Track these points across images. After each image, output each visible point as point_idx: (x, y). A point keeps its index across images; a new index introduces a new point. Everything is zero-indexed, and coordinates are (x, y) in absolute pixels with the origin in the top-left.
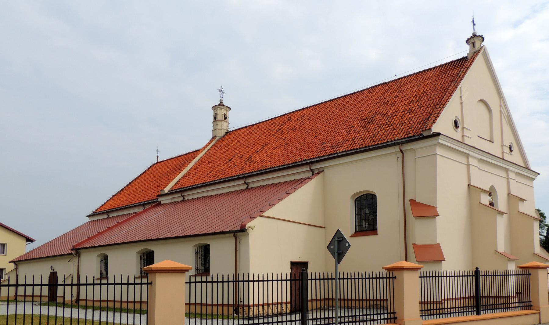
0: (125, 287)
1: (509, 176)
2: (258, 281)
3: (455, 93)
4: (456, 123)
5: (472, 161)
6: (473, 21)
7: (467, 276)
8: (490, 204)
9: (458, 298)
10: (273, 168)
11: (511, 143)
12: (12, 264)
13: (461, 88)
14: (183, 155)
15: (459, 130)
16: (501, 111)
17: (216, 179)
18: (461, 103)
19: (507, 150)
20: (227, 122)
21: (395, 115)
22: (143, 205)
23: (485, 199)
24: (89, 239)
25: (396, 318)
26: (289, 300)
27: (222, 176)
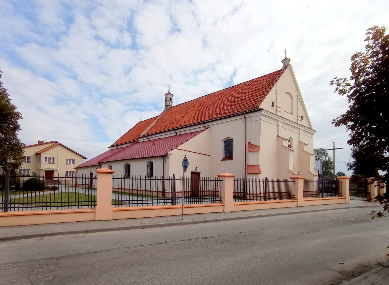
0: (207, 181)
1: (300, 131)
2: (205, 180)
3: (273, 88)
4: (273, 103)
5: (280, 124)
6: (285, 51)
7: (276, 182)
8: (289, 147)
9: (261, 193)
10: (188, 125)
11: (303, 115)
12: (75, 169)
13: (276, 86)
14: (151, 118)
15: (274, 107)
16: (297, 98)
17: (163, 130)
18: (276, 94)
19: (300, 119)
20: (171, 102)
21: (245, 99)
22: (132, 142)
23: (286, 144)
24: (106, 158)
25: (222, 200)
26: (190, 190)
27: (166, 129)
